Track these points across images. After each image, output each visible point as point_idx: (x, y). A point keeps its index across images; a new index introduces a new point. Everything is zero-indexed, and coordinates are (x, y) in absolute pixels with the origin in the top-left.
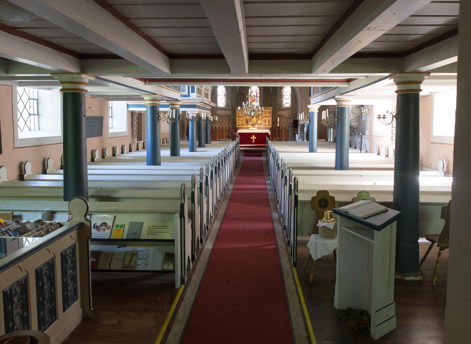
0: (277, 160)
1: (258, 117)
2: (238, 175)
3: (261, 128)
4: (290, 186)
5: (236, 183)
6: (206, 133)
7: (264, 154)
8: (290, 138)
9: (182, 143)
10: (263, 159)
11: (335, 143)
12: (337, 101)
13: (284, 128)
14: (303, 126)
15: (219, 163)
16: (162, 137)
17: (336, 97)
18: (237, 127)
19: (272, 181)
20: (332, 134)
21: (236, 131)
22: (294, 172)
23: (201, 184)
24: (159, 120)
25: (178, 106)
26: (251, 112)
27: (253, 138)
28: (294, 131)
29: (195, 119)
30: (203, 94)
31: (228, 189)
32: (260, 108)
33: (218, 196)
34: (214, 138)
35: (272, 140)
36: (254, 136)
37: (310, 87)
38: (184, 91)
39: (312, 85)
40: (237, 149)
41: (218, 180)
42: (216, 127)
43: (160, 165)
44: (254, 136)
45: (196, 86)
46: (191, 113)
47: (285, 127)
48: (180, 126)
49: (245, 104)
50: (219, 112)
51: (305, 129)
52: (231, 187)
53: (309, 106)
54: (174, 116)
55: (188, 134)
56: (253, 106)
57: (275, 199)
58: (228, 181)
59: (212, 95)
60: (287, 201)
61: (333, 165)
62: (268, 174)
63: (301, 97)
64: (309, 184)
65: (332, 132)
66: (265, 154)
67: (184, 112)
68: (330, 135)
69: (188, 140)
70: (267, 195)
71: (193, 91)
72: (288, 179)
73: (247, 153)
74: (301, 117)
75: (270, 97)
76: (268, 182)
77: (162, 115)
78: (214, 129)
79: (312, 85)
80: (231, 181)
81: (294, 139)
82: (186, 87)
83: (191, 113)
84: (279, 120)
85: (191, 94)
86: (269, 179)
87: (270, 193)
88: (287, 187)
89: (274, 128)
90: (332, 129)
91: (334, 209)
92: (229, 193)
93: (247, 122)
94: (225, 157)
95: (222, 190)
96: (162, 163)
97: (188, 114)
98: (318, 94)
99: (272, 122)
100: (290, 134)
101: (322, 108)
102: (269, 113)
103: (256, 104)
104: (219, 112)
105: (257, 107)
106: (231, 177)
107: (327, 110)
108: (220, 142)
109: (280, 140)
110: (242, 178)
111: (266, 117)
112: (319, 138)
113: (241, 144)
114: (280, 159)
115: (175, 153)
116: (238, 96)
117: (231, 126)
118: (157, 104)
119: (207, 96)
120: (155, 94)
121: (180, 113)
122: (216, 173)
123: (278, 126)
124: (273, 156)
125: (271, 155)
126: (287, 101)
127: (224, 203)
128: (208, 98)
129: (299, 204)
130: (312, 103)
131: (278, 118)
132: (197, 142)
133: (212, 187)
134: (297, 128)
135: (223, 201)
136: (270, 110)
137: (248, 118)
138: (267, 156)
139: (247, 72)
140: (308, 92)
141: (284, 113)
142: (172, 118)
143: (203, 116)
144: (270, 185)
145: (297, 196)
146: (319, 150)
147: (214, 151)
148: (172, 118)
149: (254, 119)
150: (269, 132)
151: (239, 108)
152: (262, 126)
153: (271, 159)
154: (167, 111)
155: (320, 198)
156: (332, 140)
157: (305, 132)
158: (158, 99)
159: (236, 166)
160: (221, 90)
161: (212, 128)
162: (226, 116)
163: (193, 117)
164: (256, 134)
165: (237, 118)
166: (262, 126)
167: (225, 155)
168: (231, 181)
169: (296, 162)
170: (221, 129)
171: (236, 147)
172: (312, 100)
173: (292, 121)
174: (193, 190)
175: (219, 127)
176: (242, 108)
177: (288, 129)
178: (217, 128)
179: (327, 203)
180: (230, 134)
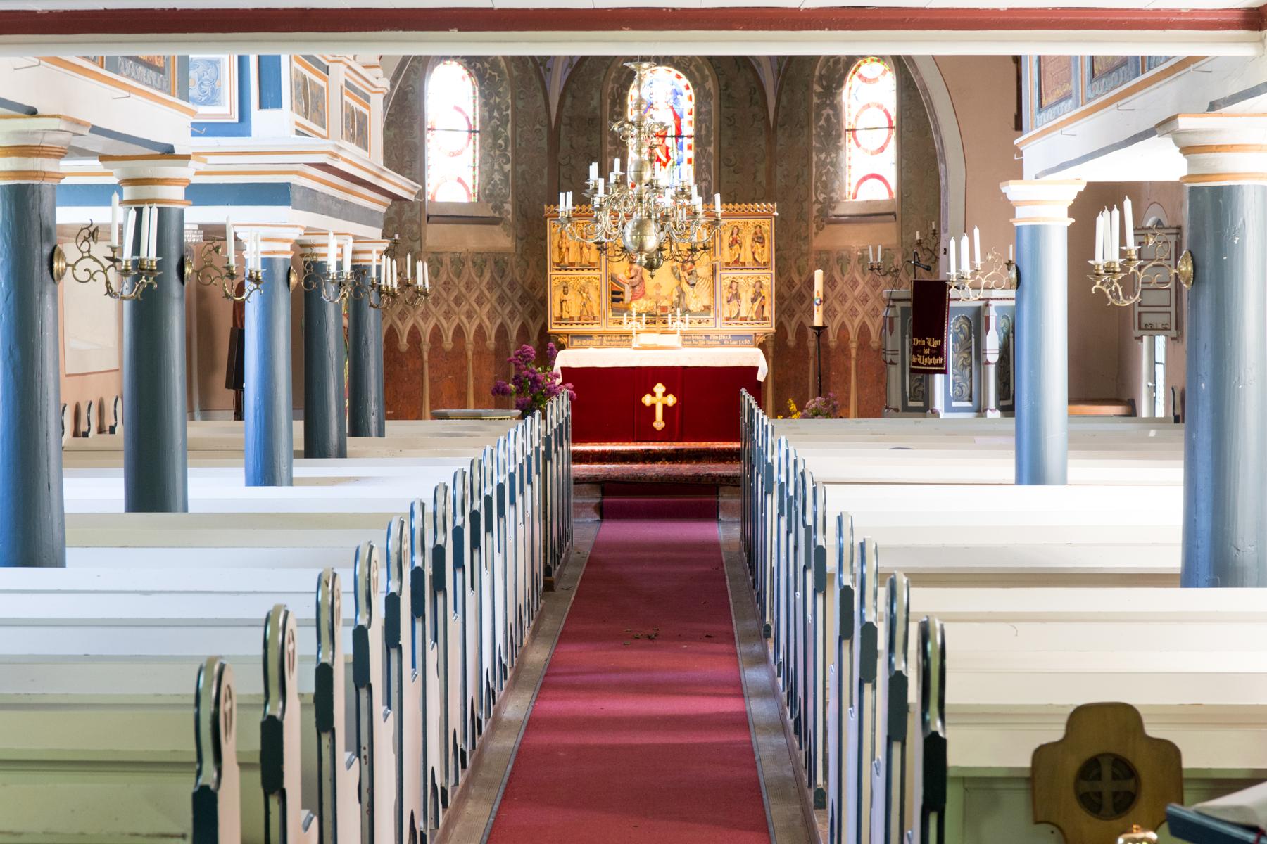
2: (565, 637)
3: (707, 340)
4: (898, 683)
5: (552, 681)
6: (354, 365)
7: (727, 499)
8: (895, 400)
9: (198, 430)
10: (725, 532)
11: (1179, 431)
12: (1186, 150)
14: (977, 321)
15: (439, 552)
17: (1184, 123)
18: (553, 328)
19: (783, 668)
20: (1160, 371)
21: (546, 358)
22: (924, 602)
23: (324, 674)
24: (54, 276)
25: (177, 193)
26: (640, 226)
27: (659, 398)
28: (917, 350)
30: (335, 115)
31: (496, 723)
32: (697, 201)
33: (435, 760)
35: (781, 411)
36: (659, 388)
37: (1017, 60)
38: (211, 99)
39: (1030, 46)
41: (433, 656)
42: (414, 334)
43: (62, 564)
44: (659, 388)
45: (291, 54)
46: (261, 235)
47: (864, 332)
48: (187, 334)
49: (603, 173)
50: (435, 236)
51: (992, 342)
52: (516, 708)
53: (1013, 190)
54: (149, 252)
55: (236, 379)
56: (653, 187)
57: (797, 778)
59: (389, 124)
60: (876, 783)
61: (1173, 561)
62: (751, 625)
64: (1016, 681)
65: (1160, 356)
66: (737, 502)
67: (214, 234)
69: (239, 414)
70: (747, 755)
71: (270, 99)
73: (618, 498)
74: (963, 259)
76: (755, 676)
77: (70, 251)
78: (404, 344)
79: (1030, 46)
80: (518, 670)
81: (918, 402)
82: (227, 57)
83: (261, 235)
84: (829, 282)
85: (257, 116)
86: (762, 660)
87: (767, 745)
88: (878, 697)
89: (791, 341)
90: (1161, 341)
91: (1174, 808)
92: (507, 743)
93: (616, 296)
94: (475, 516)
95: (455, 723)
96: (71, 554)
98: (1068, 109)
99: (780, 298)
100: (894, 373)
102: (759, 239)
103: (678, 174)
104: (435, 236)
106: (514, 644)
107: (1128, 204)
109: (833, 411)
110: (583, 655)
111: (738, 264)
113: (577, 439)
114: (832, 524)
115: (151, 488)
117: (514, 329)
118: (45, 175)
119: (357, 130)
120: (32, 112)
122: (418, 611)
123: (818, 321)
124: (788, 507)
125: (773, 502)
126: (866, 166)
127: (470, 808)
129: (953, 795)
130: (1030, 168)
131: (819, 275)
132: (299, 426)
133: (393, 698)
134: (939, 334)
135: (463, 797)
136: (760, 220)
137: (621, 269)
138: (749, 516)
140: (1008, 96)
141: (853, 240)
142: (138, 264)
144: (768, 693)
145: (943, 742)
146: (1081, 469)
147: (404, 475)
148: (138, 264)
149: (664, 281)
151: (566, 202)
153: (774, 527)
155: (1087, 754)
156: (1160, 412)
157: (993, 357)
158: (50, 140)
159: (547, 581)
160: (451, 99)
161: (391, 336)
162: (482, 260)
163: (268, 263)
164: (674, 377)
165: (555, 278)
166: (715, 325)
167: (478, 505)
168: (513, 671)
170: (448, 344)
171: (547, 456)
172: (1036, 150)
173: (906, 291)
174: (274, 709)
175: (437, 334)
178: (426, 338)
179: (1129, 785)
180: (506, 377)
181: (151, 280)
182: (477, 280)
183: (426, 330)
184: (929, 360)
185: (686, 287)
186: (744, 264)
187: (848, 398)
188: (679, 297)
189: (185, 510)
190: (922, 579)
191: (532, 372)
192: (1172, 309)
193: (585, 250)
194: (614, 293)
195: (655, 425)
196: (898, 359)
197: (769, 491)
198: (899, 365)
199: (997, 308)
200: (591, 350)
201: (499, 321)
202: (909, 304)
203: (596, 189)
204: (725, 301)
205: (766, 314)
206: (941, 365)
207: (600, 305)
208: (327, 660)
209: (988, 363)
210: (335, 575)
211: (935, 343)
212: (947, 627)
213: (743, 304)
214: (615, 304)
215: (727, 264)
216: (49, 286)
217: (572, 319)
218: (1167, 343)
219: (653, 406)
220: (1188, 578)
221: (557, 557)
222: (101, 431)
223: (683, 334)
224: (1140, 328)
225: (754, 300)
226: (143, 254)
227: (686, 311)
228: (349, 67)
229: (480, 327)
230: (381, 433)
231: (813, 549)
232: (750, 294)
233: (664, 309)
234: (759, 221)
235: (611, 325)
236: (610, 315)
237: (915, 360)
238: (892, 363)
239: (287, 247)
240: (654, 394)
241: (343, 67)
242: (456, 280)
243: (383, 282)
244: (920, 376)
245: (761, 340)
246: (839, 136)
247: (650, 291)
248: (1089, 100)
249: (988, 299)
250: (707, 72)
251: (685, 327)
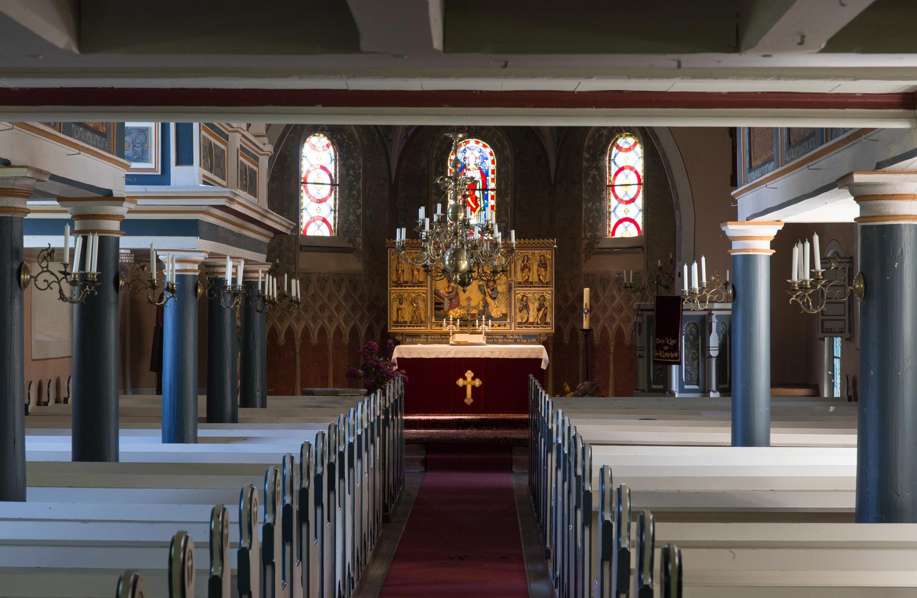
0: (580, 480)
1: (489, 289)
2: (398, 558)
3: (505, 339)
6: (243, 352)
8: (643, 383)
9: (127, 401)
10: (517, 480)
11: (854, 408)
12: (858, 199)
13: (611, 334)
15: (304, 493)
16: (33, 374)
18: (393, 329)
19: (559, 582)
20: (837, 362)
22: (665, 532)
24: (22, 285)
25: (115, 225)
27: (469, 381)
28: (659, 347)
29: (190, 287)
34: (281, 382)
35: (558, 391)
36: (469, 374)
37: (733, 131)
39: (743, 121)
40: (390, 432)
42: (290, 332)
43: (21, 498)
44: (469, 374)
46: (176, 256)
47: (619, 333)
49: (429, 214)
50: (305, 261)
51: (714, 341)
53: (731, 229)
54: (92, 267)
55: (157, 366)
56: (466, 224)
58: (348, 580)
61: (849, 502)
63: (696, 179)
65: (837, 352)
67: (142, 256)
68: (832, 368)
69: (159, 391)
72: (633, 564)
73: (437, 453)
74: (694, 276)
75: (550, 181)
78: (282, 339)
79: (743, 121)
81: (659, 386)
83: (176, 256)
84: (593, 297)
89: (566, 339)
90: (838, 341)
93: (438, 306)
94: (331, 467)
96: (30, 491)
97: (160, 265)
99: (558, 309)
100: (642, 364)
101: (790, 236)
103: (482, 216)
105: (486, 229)
106: (359, 561)
108: (307, 399)
109: (597, 391)
111: (527, 283)
112: (777, 380)
114: (596, 474)
115: (93, 445)
116: (395, 177)
117: (363, 330)
119: (249, 182)
121: (124, 259)
123: (586, 325)
125: (552, 459)
126: (625, 212)
128: (253, 192)
131: (586, 291)
132: (203, 400)
134: (676, 337)
137: (442, 286)
138: (535, 469)
139: (437, 43)
141: (611, 266)
142: (84, 276)
143: (232, 272)
147: (274, 440)
148: (84, 276)
149: (473, 295)
150: (545, 356)
151: (401, 235)
152: (510, 328)
154: (61, 250)
156: (837, 393)
157: (714, 353)
158: (20, 184)
160: (318, 157)
161: (273, 334)
163: (181, 278)
164: (479, 365)
165: (393, 292)
169: (673, 488)
170: (314, 340)
171: (386, 423)
172: (746, 202)
173: (650, 303)
175: (306, 333)
176: (414, 234)
177: (639, 339)
178: (298, 336)
181: (93, 289)
182: (336, 293)
183: (299, 329)
184: (667, 355)
185: (489, 299)
186: (532, 283)
187: (608, 383)
188: (484, 307)
189: (117, 460)
190: (664, 516)
191: (376, 361)
192: (846, 317)
193: (416, 272)
194: (436, 304)
195: (466, 401)
196: (645, 354)
197: (549, 450)
198: (646, 358)
199: (717, 316)
200: (419, 346)
201: (352, 324)
202: (653, 313)
203: (423, 226)
204: (517, 311)
205: (548, 320)
206: (677, 358)
207: (426, 312)
208: (218, 573)
209: (711, 357)
210: (224, 510)
211: (672, 342)
212: (683, 551)
213: (531, 313)
214: (437, 312)
215: (520, 283)
216: (18, 292)
217: (405, 322)
218: (842, 342)
219: (465, 387)
220: (861, 515)
221: (392, 498)
222: (57, 401)
223: (487, 334)
224: (823, 332)
225: (539, 310)
226: (88, 270)
227: (489, 317)
228: (243, 136)
229: (338, 328)
230: (264, 405)
231: (582, 493)
232: (537, 304)
233: (473, 315)
234: (543, 252)
235: (434, 327)
236: (433, 320)
237: (657, 354)
238: (640, 356)
239: (196, 267)
240: (465, 378)
241: (239, 136)
242: (321, 294)
243: (266, 293)
244: (660, 366)
245: (544, 339)
246: (602, 190)
247: (463, 303)
248: (787, 162)
249: (711, 310)
250: (505, 143)
251: (488, 329)
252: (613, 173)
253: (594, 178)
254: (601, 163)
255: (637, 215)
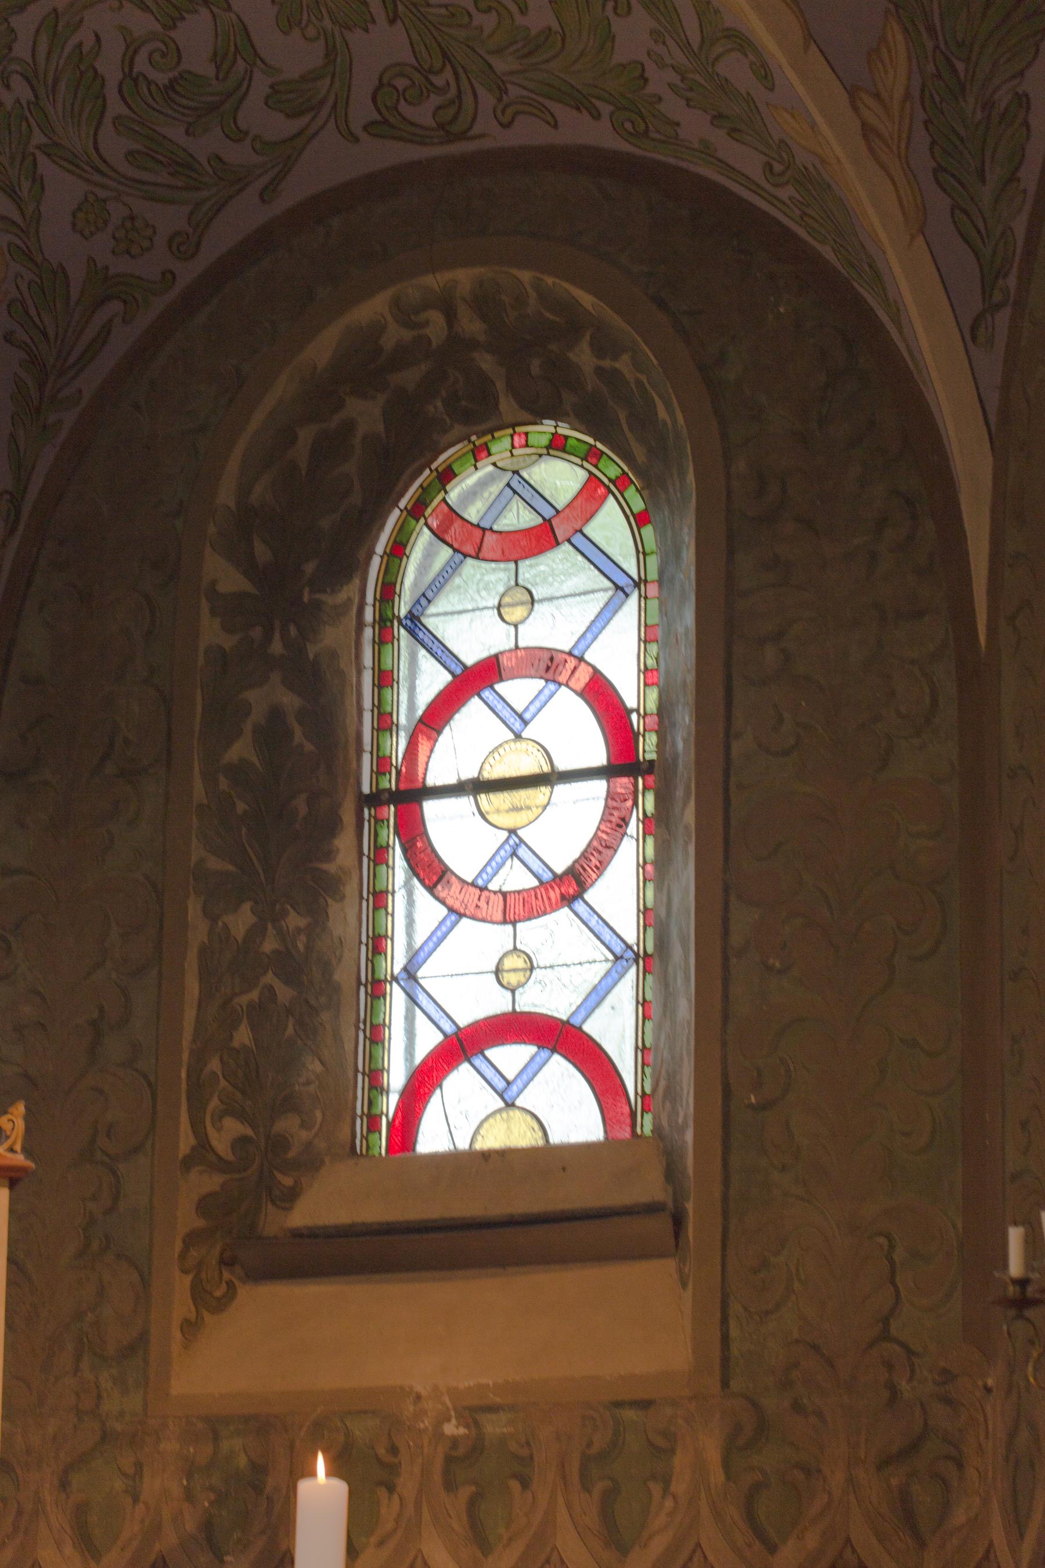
246: (332, 826)
252: (397, 1077)
253: (273, 733)
254: (330, 636)
255: (597, 996)
